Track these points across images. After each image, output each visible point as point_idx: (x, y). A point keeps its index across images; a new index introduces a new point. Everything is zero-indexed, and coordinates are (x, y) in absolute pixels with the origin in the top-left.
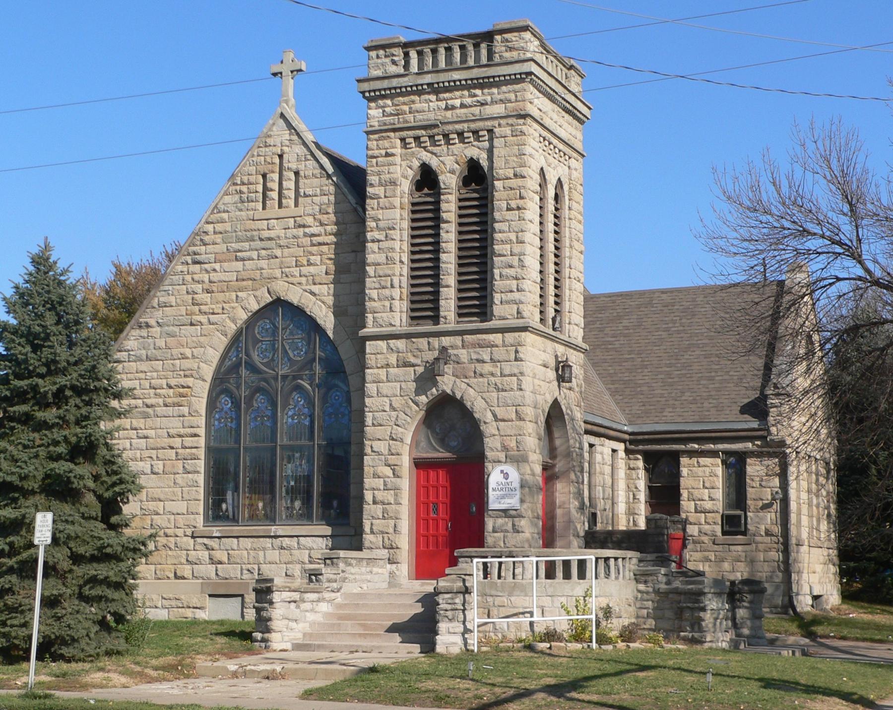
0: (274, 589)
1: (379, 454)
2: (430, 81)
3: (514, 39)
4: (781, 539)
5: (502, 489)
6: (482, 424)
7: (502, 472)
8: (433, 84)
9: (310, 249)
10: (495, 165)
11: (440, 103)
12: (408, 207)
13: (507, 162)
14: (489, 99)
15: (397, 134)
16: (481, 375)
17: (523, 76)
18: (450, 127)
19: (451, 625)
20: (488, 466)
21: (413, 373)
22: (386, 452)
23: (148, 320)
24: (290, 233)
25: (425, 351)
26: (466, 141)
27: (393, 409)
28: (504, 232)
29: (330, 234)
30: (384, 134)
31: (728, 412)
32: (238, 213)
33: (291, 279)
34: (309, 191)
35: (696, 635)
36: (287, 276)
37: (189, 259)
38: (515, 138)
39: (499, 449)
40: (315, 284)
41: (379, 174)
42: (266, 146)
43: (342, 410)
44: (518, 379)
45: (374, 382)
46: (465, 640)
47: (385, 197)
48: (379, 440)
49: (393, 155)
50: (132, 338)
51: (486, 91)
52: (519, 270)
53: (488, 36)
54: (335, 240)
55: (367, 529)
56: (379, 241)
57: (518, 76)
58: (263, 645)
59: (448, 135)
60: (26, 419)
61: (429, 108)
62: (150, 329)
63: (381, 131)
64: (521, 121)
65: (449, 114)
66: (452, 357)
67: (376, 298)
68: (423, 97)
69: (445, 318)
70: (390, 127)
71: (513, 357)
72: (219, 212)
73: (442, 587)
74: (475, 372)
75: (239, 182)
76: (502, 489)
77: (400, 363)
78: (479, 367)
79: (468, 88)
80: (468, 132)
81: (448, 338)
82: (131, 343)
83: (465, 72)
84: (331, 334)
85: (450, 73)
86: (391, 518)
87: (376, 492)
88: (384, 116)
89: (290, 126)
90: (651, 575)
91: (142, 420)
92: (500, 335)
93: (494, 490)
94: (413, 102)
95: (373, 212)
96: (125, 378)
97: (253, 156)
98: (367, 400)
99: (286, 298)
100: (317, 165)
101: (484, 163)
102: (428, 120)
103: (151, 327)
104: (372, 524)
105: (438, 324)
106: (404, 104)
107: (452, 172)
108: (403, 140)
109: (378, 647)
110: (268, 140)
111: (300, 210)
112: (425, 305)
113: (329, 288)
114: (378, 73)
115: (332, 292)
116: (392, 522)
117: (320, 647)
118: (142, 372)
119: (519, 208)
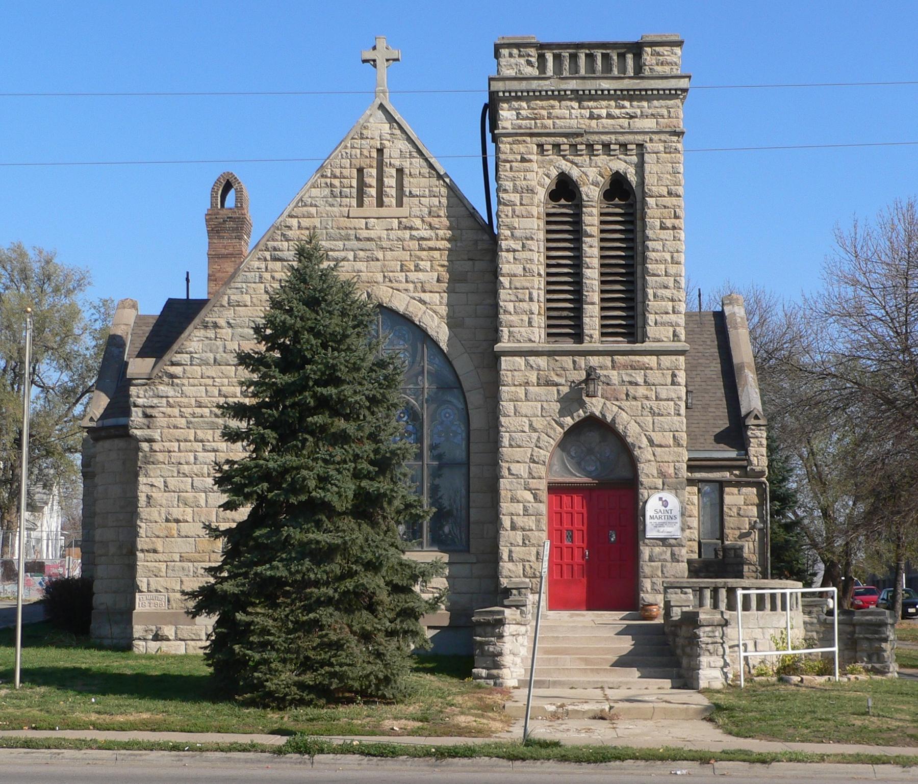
0: (507, 621)
1: (517, 477)
2: (575, 87)
3: (666, 53)
4: (759, 568)
5: (660, 518)
6: (636, 449)
7: (660, 499)
8: (578, 91)
9: (418, 253)
10: (646, 181)
11: (583, 111)
12: (543, 216)
13: (659, 179)
14: (638, 112)
15: (534, 139)
16: (635, 398)
17: (679, 92)
18: (596, 138)
19: (712, 659)
20: (644, 492)
21: (556, 392)
22: (526, 476)
23: (217, 320)
24: (393, 235)
25: (571, 371)
26: (612, 153)
27: (533, 428)
28: (657, 251)
29: (442, 239)
30: (519, 138)
31: (702, 441)
32: (328, 208)
33: (395, 285)
34: (416, 191)
35: (877, 666)
36: (390, 281)
37: (267, 255)
38: (668, 155)
39: (656, 475)
40: (424, 291)
41: (513, 179)
42: (362, 138)
43: (453, 428)
44: (675, 404)
45: (511, 400)
46: (725, 674)
47: (521, 204)
48: (518, 462)
49: (530, 161)
50: (195, 339)
51: (635, 103)
52: (675, 292)
53: (637, 49)
54: (449, 246)
55: (505, 556)
56: (514, 251)
57: (673, 92)
58: (492, 682)
59: (592, 145)
60: (320, 432)
61: (571, 116)
62: (218, 330)
63: (516, 134)
64: (675, 138)
65: (594, 123)
66: (602, 378)
67: (512, 311)
68: (563, 103)
69: (591, 337)
70: (528, 131)
71: (669, 380)
72: (306, 205)
73: (705, 619)
74: (627, 395)
75: (329, 175)
76: (660, 518)
77: (542, 381)
78: (632, 390)
79: (616, 98)
80: (615, 144)
81: (596, 358)
82: (194, 344)
83: (614, 81)
84: (444, 346)
85: (598, 81)
86: (533, 545)
87: (515, 518)
88: (518, 118)
89: (391, 119)
90: (816, 606)
91: (211, 432)
92: (655, 358)
93: (651, 518)
94: (553, 107)
95: (508, 220)
96: (186, 383)
97: (346, 147)
98: (502, 419)
99: (389, 305)
100: (424, 164)
101: (632, 178)
102: (565, 127)
103: (220, 328)
104: (510, 551)
105: (581, 342)
106: (543, 108)
107: (595, 184)
108: (540, 146)
109: (627, 683)
110: (365, 132)
111: (404, 211)
112: (566, 321)
113: (442, 298)
114: (511, 73)
115: (445, 301)
116: (534, 550)
117: (555, 684)
118: (208, 377)
119: (674, 228)
